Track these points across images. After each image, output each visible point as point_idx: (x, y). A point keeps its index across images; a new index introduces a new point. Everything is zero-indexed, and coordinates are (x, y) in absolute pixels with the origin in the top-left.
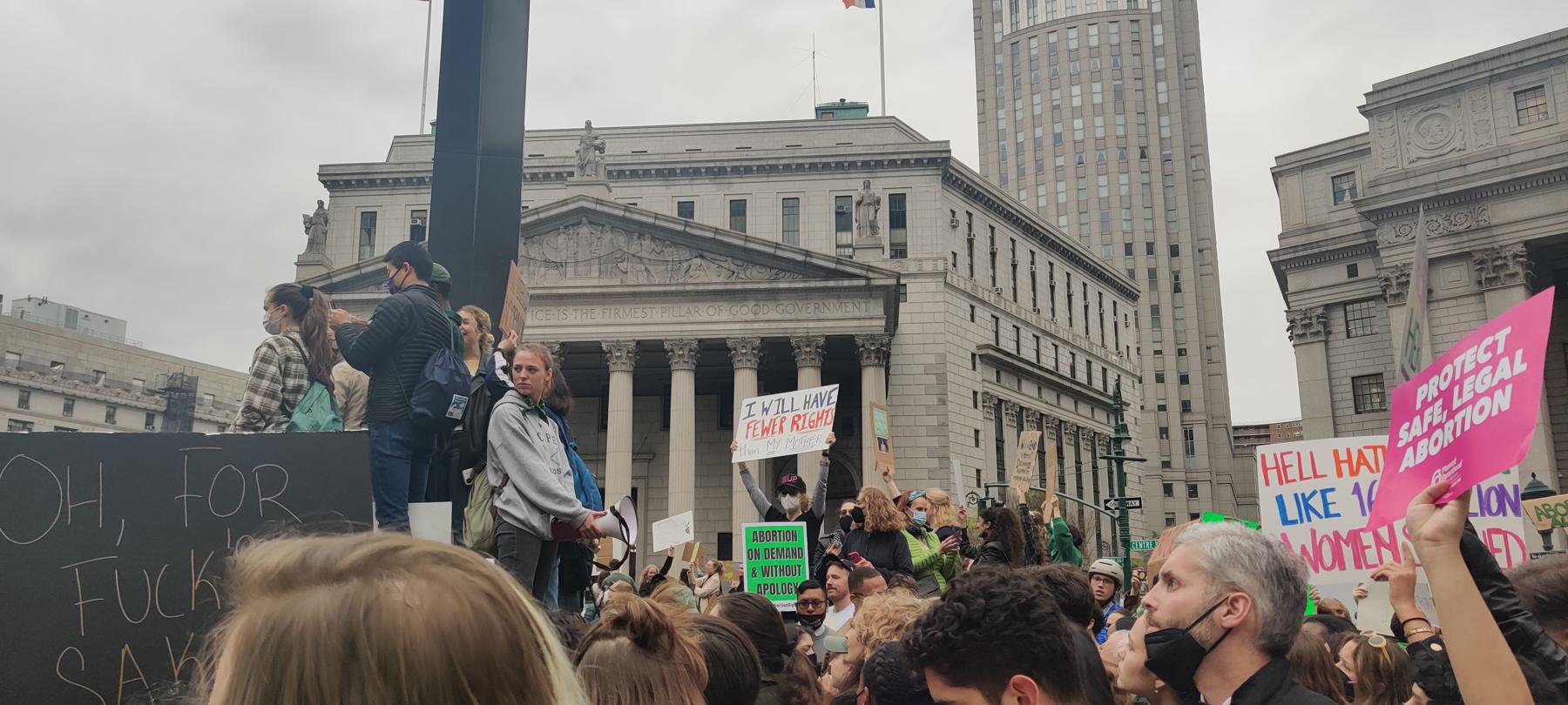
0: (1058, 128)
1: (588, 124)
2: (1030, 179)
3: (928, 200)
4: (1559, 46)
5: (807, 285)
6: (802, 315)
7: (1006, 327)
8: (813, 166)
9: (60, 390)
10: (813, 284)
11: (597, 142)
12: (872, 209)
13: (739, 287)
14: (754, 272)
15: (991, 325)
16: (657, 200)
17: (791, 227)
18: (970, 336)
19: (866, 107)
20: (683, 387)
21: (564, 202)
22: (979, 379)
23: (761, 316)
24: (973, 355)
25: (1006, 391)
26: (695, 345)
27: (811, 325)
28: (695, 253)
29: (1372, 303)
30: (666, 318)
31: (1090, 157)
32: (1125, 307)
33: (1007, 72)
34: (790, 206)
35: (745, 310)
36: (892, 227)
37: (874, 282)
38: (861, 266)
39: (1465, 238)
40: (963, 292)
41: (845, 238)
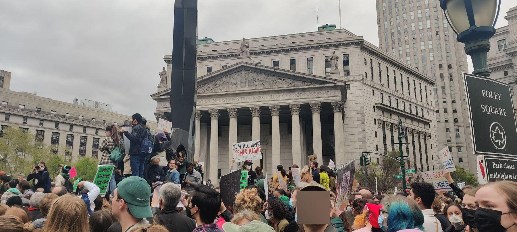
0: (406, 27)
1: (244, 39)
2: (396, 45)
3: (356, 55)
4: (514, 12)
5: (315, 86)
7: (386, 96)
8: (317, 47)
9: (94, 126)
10: (316, 86)
11: (246, 44)
12: (336, 60)
13: (292, 88)
14: (297, 83)
15: (380, 96)
16: (267, 61)
17: (310, 68)
18: (373, 100)
19: (335, 26)
20: (275, 121)
21: (237, 64)
22: (376, 114)
23: (300, 97)
24: (374, 107)
25: (387, 118)
26: (279, 107)
27: (316, 99)
28: (278, 78)
29: (513, 84)
30: (269, 99)
31: (417, 36)
32: (429, 87)
33: (387, 9)
34: (310, 60)
35: (294, 95)
36: (344, 65)
38: (332, 79)
40: (370, 86)
41: (329, 70)
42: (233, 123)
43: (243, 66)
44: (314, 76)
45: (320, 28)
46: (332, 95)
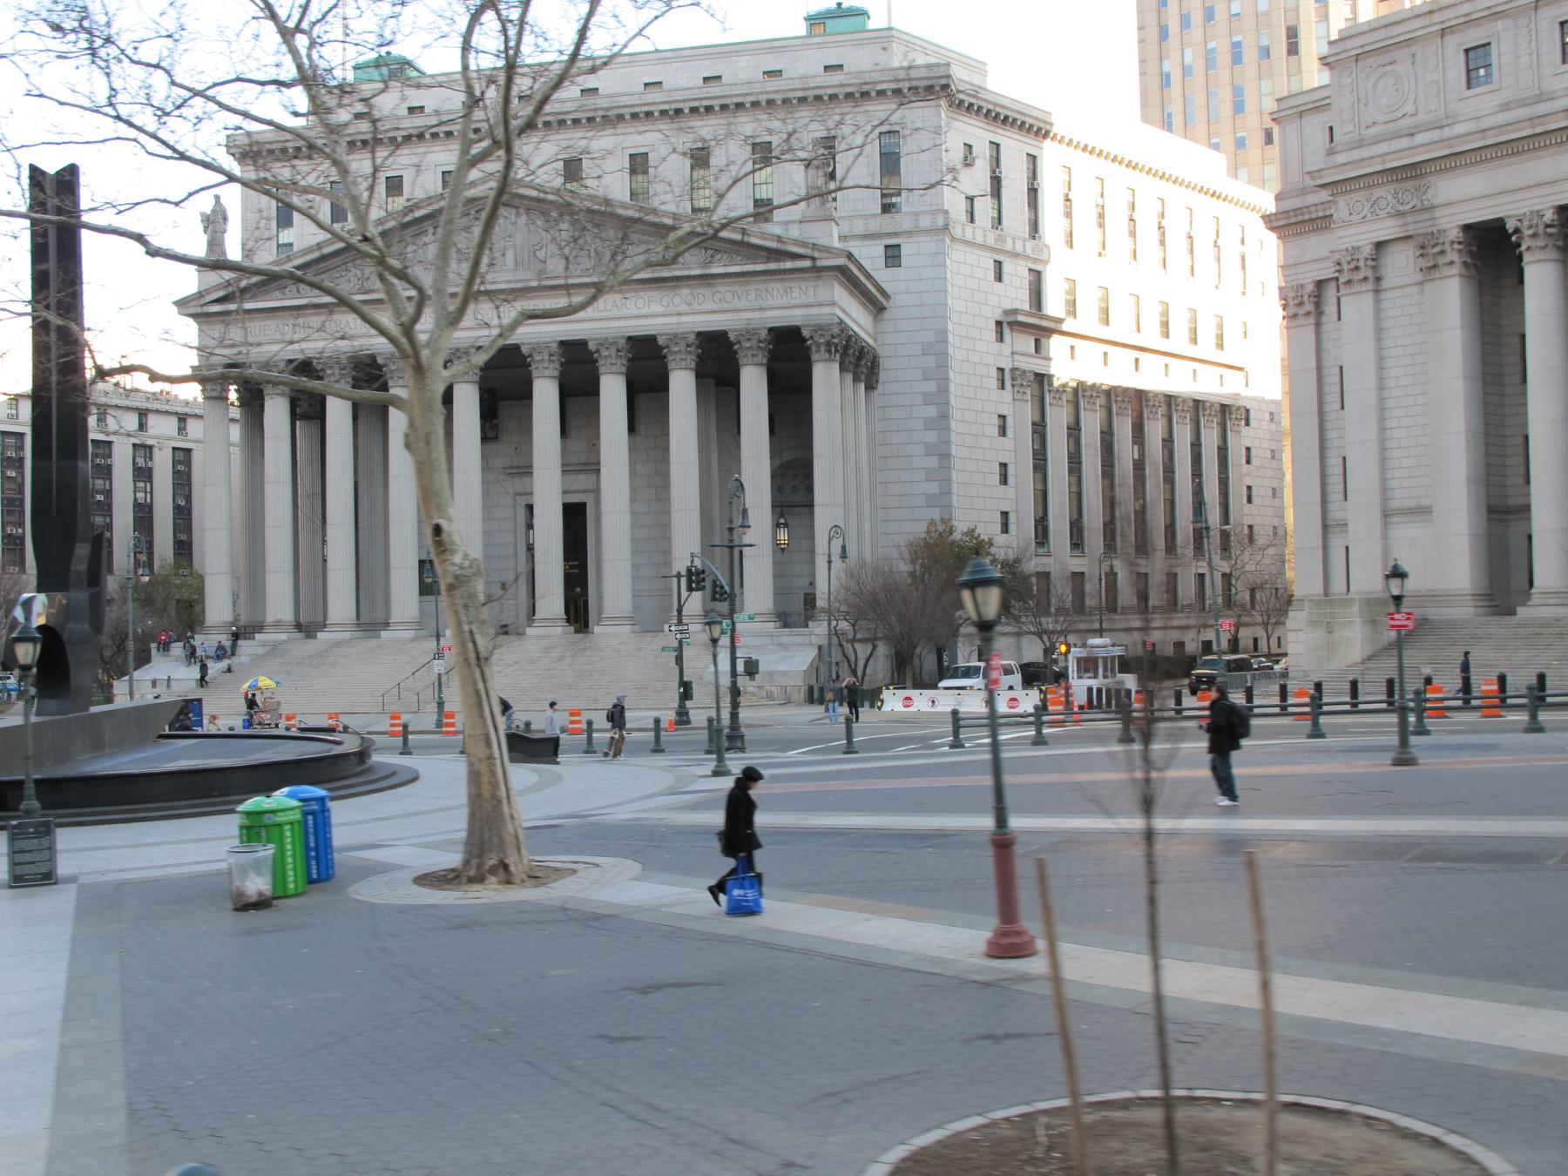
6: (743, 304)
19: (861, 13)
20: (753, 385)
23: (696, 307)
24: (999, 324)
27: (750, 315)
35: (677, 300)
37: (819, 263)
39: (1410, 219)
46: (804, 300)
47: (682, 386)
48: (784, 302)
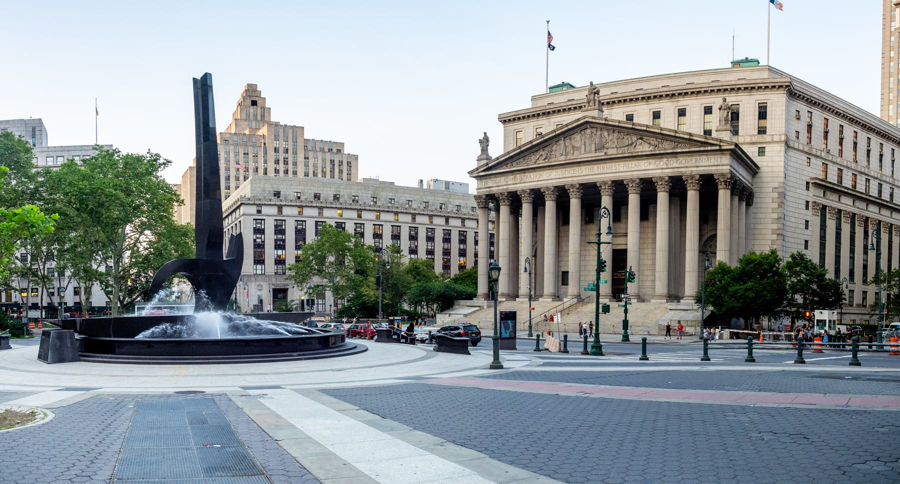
1: (591, 83)
6: (690, 164)
10: (693, 149)
16: (617, 114)
18: (805, 173)
20: (693, 197)
21: (578, 120)
24: (808, 183)
25: (831, 201)
26: (638, 181)
27: (693, 169)
30: (625, 169)
35: (662, 163)
37: (723, 148)
38: (716, 140)
42: (575, 204)
43: (587, 122)
44: (661, 129)
45: (736, 64)
47: (662, 198)
48: (707, 164)
